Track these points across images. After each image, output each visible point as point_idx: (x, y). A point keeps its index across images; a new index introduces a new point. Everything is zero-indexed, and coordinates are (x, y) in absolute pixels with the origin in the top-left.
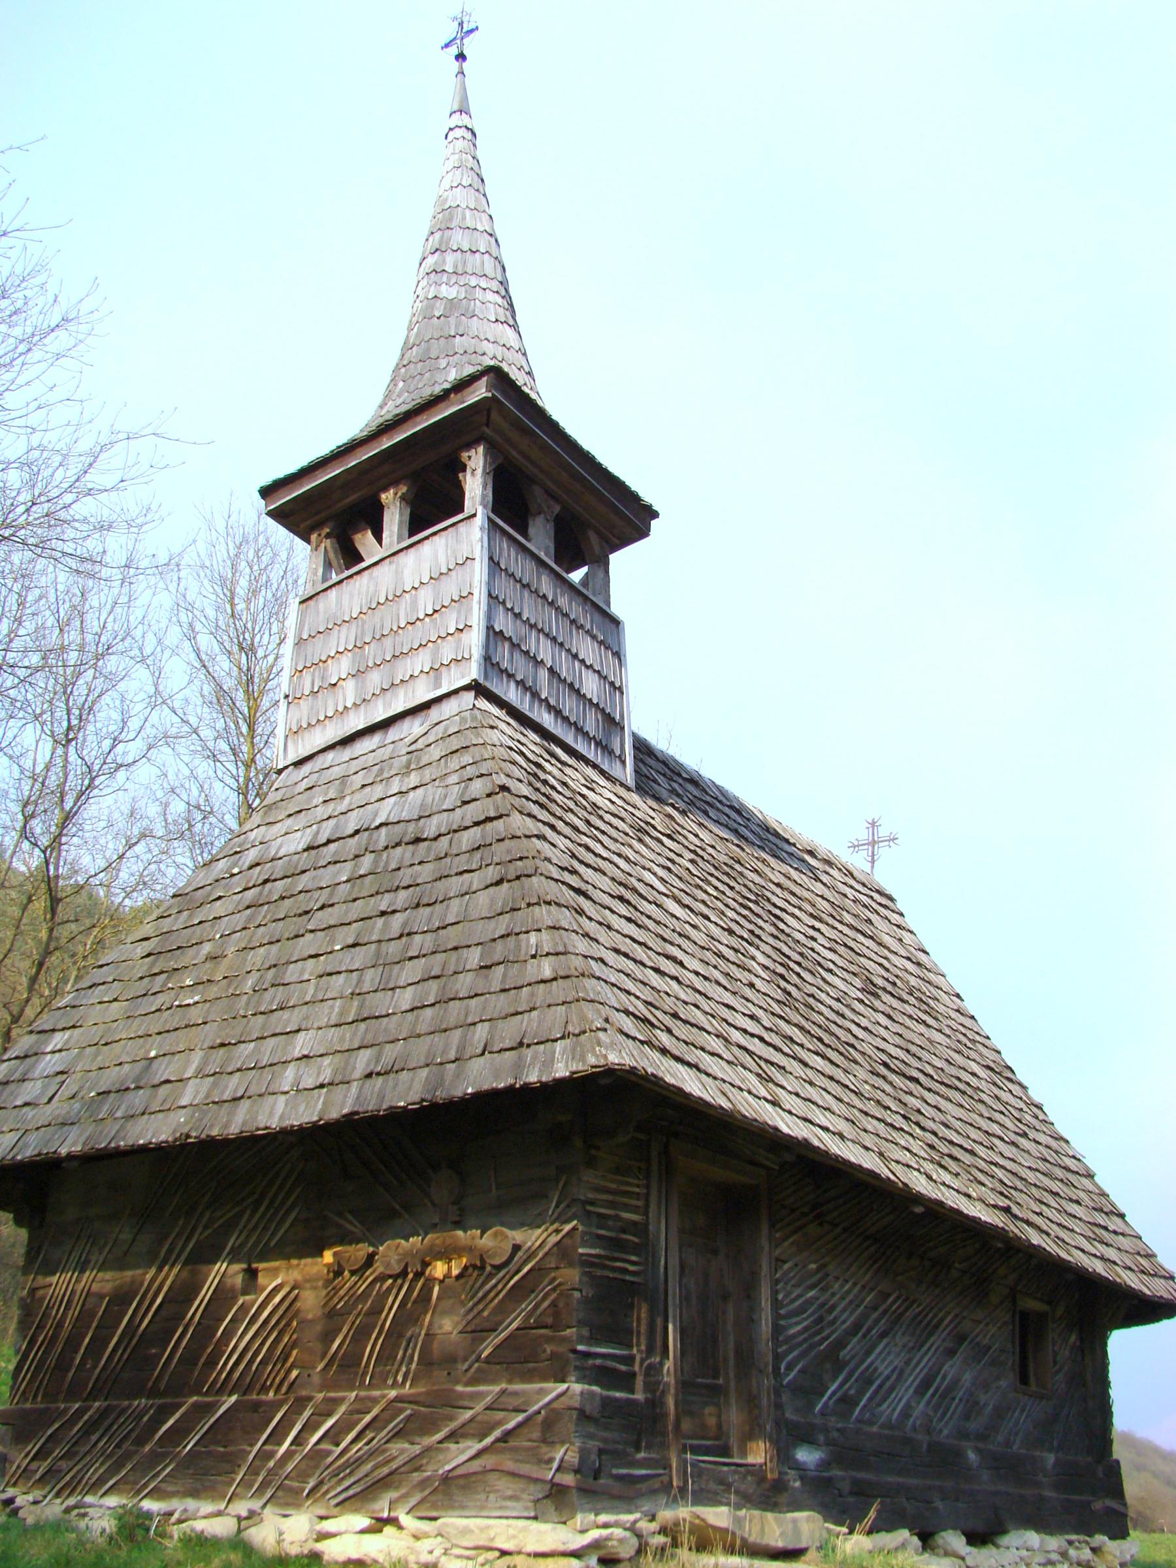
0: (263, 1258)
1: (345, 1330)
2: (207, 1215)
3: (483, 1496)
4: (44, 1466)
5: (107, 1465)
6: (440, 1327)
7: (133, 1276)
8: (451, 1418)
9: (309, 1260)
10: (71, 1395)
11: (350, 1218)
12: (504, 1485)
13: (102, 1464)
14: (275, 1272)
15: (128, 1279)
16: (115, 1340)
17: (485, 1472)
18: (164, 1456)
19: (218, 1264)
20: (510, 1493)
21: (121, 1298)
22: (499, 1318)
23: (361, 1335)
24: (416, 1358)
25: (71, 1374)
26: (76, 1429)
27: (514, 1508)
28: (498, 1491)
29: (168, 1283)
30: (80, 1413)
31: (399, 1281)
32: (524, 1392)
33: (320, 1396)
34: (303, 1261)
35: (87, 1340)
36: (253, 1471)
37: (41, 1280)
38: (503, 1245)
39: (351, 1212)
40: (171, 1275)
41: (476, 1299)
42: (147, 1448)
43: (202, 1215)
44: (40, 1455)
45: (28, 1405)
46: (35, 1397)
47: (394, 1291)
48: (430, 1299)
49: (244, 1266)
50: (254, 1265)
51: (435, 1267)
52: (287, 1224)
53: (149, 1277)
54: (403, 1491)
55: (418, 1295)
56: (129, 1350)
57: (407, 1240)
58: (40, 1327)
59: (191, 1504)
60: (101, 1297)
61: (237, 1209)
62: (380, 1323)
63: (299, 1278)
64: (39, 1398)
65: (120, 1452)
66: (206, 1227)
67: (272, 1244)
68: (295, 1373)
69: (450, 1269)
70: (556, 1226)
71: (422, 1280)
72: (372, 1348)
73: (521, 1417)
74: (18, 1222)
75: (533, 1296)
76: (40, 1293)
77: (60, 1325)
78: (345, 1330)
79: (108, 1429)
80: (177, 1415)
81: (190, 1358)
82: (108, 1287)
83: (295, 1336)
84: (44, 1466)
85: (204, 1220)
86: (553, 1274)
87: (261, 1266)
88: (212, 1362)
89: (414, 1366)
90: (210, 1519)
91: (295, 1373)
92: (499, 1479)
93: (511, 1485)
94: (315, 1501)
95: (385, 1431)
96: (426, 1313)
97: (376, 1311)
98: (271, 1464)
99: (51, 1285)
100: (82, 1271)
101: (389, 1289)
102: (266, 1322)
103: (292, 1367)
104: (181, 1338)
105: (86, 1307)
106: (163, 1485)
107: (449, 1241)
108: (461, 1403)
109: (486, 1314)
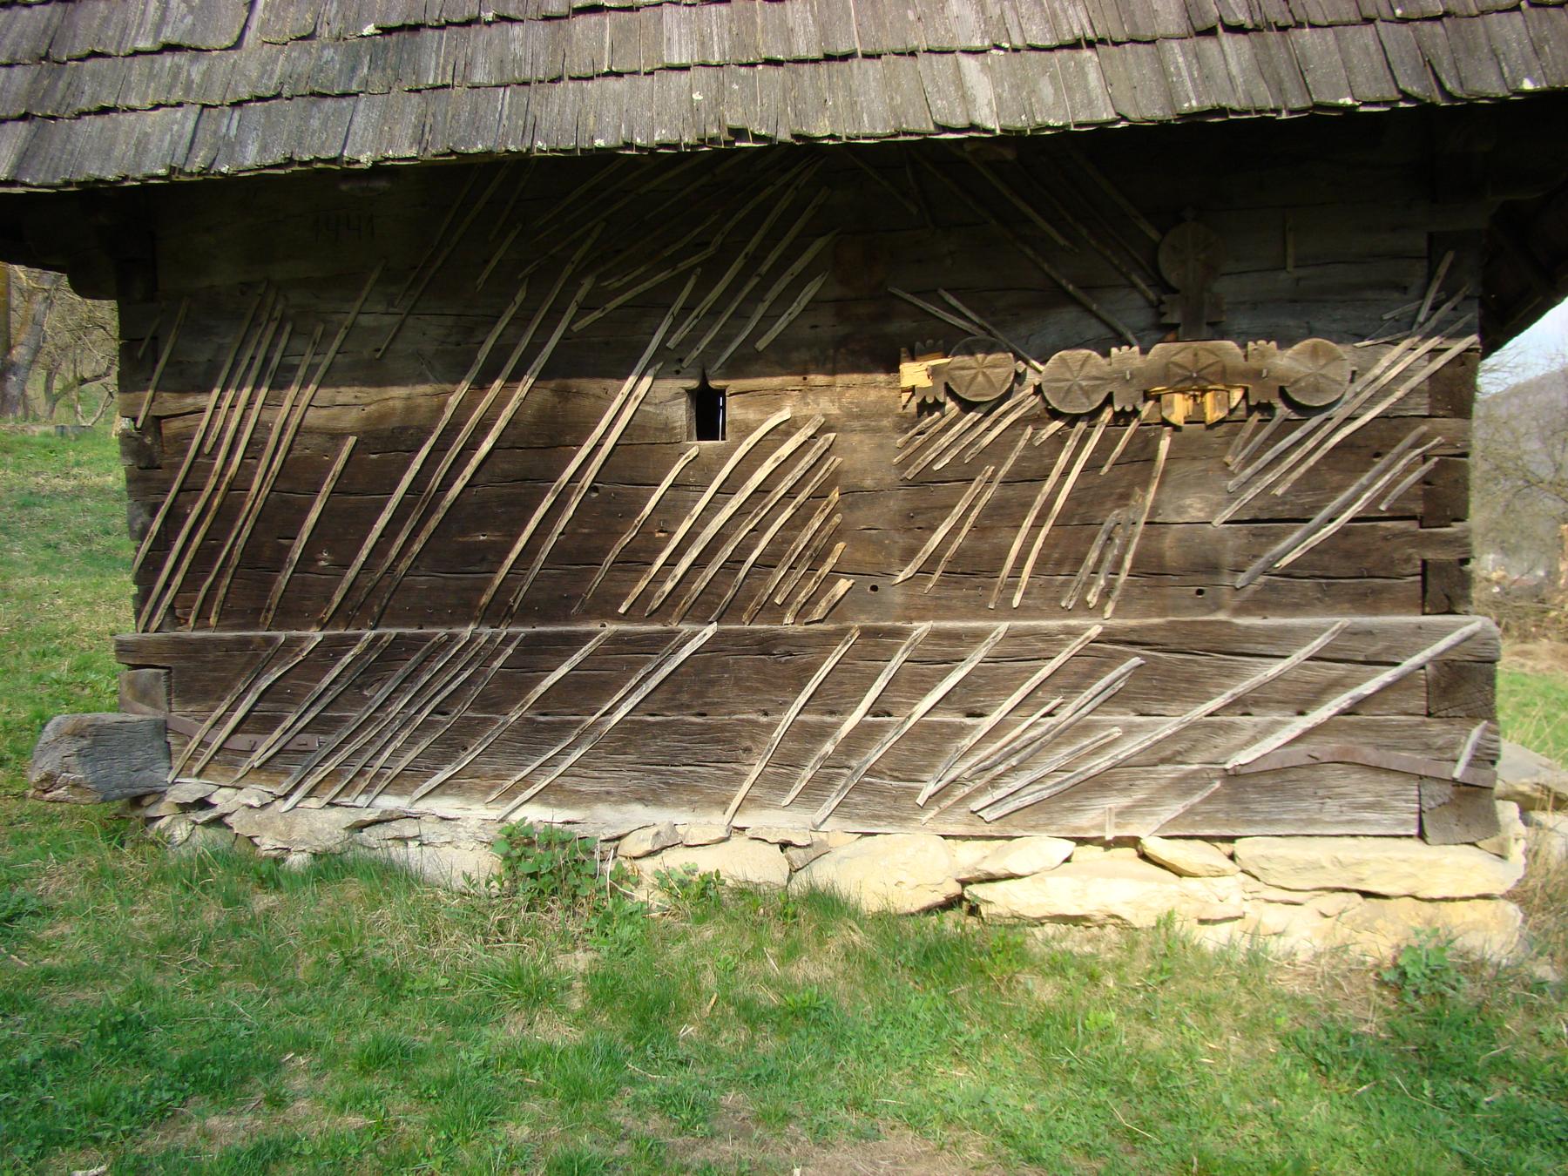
0: (736, 368)
1: (958, 510)
2: (587, 284)
3: (1313, 805)
4: (266, 746)
5: (424, 744)
6: (1180, 510)
7: (409, 398)
8: (1233, 674)
9: (856, 378)
10: (290, 613)
11: (954, 302)
12: (1356, 785)
13: (411, 742)
14: (773, 399)
15: (399, 404)
16: (385, 517)
17: (1315, 763)
18: (561, 729)
19: (632, 379)
20: (1369, 798)
21: (387, 442)
22: (1307, 499)
23: (1003, 514)
24: (1127, 564)
25: (283, 579)
26: (327, 680)
27: (1378, 823)
28: (1343, 795)
29: (507, 413)
30: (332, 649)
31: (1081, 426)
32: (1385, 632)
33: (922, 628)
34: (842, 379)
35: (313, 517)
36: (788, 761)
37: (171, 402)
38: (1331, 371)
39: (953, 291)
40: (514, 399)
41: (1259, 464)
42: (513, 716)
43: (574, 282)
44: (258, 722)
45: (188, 633)
46: (203, 616)
47: (1071, 443)
48: (1152, 460)
49: (693, 384)
50: (715, 384)
51: (1171, 404)
52: (796, 308)
53: (453, 401)
54: (1139, 795)
55: (1124, 453)
56: (423, 537)
57: (1106, 354)
58: (190, 489)
59: (661, 817)
60: (337, 437)
61: (661, 277)
62: (1040, 500)
63: (834, 410)
64: (213, 620)
65: (447, 721)
66: (584, 309)
67: (761, 345)
68: (843, 586)
69: (1200, 407)
70: (1433, 342)
71: (1134, 424)
72: (1026, 543)
73: (1388, 675)
74: (85, 286)
75: (1381, 463)
76: (174, 426)
77: (239, 485)
78: (958, 510)
79: (410, 678)
80: (577, 658)
81: (578, 553)
82: (350, 419)
83: (837, 519)
84: (266, 746)
85: (581, 294)
86: (1424, 428)
87: (733, 385)
88: (635, 559)
89: (1123, 577)
90: (727, 840)
91: (843, 586)
92: (1347, 776)
93: (1370, 787)
94: (942, 812)
95: (1089, 693)
96: (1145, 485)
97: (1031, 475)
98: (829, 747)
99: (202, 410)
100: (279, 385)
101: (1059, 440)
102: (762, 491)
103: (835, 575)
104: (546, 520)
105: (296, 453)
106: (569, 782)
107: (1206, 359)
108: (1250, 647)
109: (1279, 491)
